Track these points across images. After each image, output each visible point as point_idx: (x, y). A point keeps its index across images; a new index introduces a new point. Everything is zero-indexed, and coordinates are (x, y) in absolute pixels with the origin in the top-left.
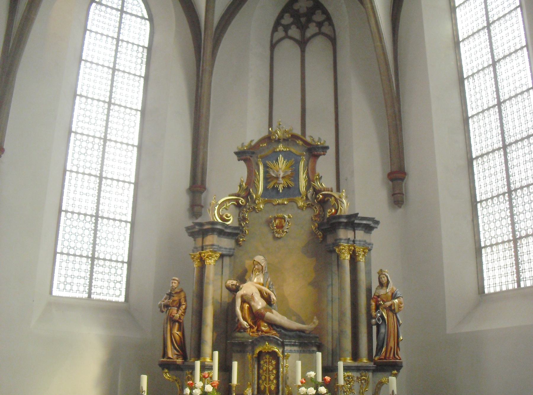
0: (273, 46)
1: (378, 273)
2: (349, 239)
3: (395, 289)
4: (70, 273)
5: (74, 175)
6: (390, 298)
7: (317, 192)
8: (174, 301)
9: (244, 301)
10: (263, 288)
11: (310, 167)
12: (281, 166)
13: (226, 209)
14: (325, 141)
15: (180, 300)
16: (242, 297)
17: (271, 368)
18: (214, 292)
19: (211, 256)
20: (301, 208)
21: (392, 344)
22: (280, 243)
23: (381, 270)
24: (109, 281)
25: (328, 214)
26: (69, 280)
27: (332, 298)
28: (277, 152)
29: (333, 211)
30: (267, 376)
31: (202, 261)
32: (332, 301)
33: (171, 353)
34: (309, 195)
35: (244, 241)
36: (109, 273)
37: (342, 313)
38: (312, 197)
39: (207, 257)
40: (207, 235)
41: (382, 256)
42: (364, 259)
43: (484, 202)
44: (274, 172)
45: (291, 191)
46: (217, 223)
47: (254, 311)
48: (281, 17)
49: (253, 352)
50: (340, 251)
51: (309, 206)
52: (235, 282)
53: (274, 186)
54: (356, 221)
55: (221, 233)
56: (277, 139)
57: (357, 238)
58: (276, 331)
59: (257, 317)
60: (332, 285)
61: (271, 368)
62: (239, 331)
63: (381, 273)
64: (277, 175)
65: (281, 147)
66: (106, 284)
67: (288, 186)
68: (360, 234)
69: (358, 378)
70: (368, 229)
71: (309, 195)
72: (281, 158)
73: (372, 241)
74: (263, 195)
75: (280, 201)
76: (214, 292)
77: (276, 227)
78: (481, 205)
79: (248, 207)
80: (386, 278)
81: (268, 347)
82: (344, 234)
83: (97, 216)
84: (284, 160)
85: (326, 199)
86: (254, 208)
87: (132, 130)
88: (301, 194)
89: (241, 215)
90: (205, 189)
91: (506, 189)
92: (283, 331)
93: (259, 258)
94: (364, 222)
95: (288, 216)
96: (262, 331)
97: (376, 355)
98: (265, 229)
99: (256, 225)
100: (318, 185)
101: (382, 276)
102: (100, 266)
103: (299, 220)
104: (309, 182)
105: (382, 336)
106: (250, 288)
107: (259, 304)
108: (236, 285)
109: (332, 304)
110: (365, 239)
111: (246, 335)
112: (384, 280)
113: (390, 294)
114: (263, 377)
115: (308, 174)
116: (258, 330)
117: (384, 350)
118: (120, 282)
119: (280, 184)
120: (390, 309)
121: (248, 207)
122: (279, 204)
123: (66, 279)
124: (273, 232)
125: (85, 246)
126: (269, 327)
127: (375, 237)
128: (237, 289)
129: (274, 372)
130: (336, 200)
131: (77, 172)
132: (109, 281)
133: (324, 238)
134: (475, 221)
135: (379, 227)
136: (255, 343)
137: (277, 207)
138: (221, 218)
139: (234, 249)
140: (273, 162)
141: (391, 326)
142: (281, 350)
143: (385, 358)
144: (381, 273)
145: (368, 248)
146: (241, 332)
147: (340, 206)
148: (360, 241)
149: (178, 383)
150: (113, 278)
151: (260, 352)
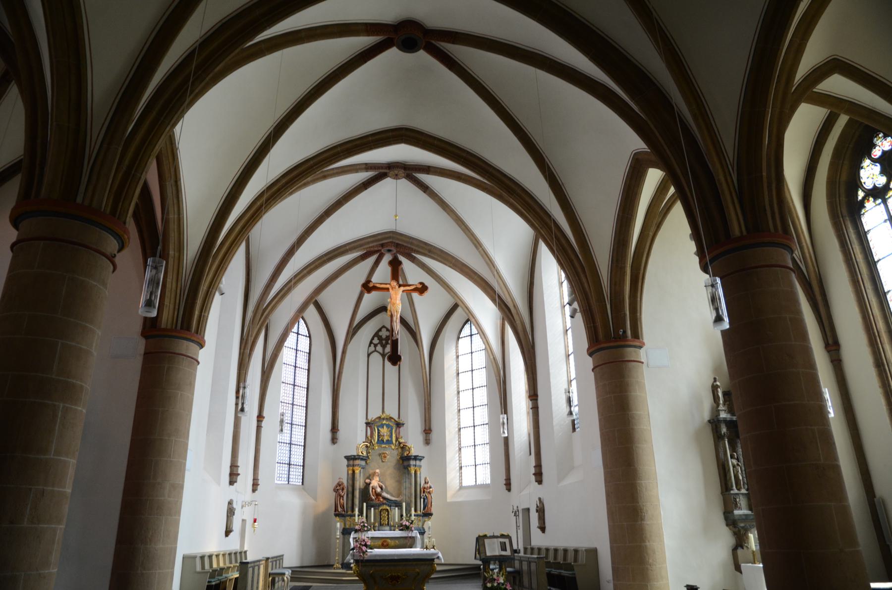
0: (369, 355)
7: (400, 443)
18: (360, 483)
31: (354, 471)
33: (340, 509)
37: (411, 494)
41: (424, 472)
48: (373, 339)
55: (362, 459)
59: (378, 495)
63: (425, 479)
65: (384, 422)
68: (418, 462)
76: (360, 483)
77: (382, 456)
81: (385, 507)
82: (412, 462)
83: (290, 444)
93: (378, 471)
100: (401, 441)
103: (392, 454)
104: (397, 439)
107: (379, 490)
120: (429, 493)
127: (423, 463)
134: (478, 279)
136: (379, 505)
144: (425, 479)
145: (420, 466)
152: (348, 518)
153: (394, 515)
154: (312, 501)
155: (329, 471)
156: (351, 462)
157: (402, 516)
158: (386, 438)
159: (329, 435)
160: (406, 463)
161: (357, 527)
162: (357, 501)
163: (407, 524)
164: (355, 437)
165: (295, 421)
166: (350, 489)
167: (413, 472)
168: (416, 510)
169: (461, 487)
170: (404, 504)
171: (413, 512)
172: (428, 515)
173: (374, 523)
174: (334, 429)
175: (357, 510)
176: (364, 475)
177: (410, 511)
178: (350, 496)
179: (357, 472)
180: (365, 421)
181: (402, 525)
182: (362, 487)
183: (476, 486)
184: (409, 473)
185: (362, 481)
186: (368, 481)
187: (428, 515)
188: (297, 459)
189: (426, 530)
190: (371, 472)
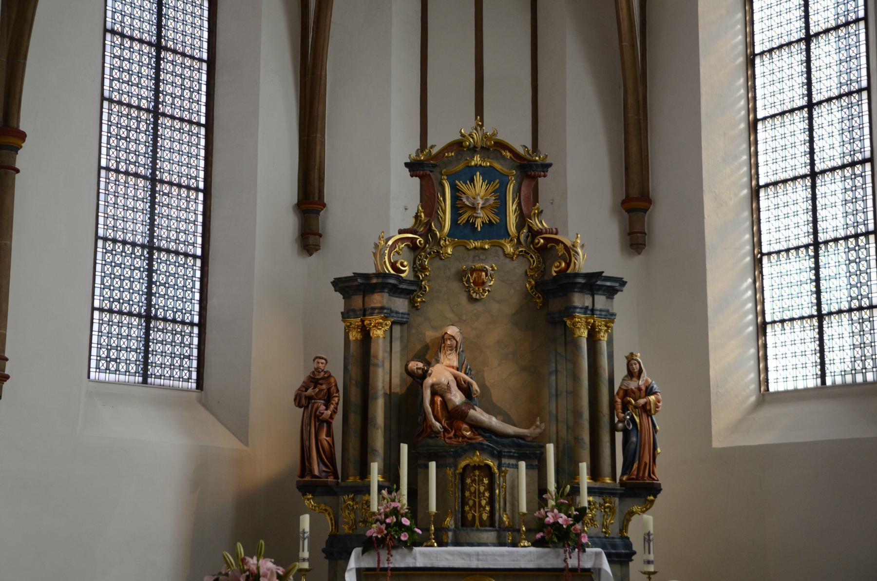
1: (627, 358)
2: (587, 307)
3: (650, 381)
4: (114, 342)
5: (113, 176)
6: (643, 394)
7: (534, 234)
8: (321, 390)
9: (434, 393)
10: (459, 373)
11: (522, 194)
12: (479, 191)
13: (398, 253)
14: (546, 156)
15: (329, 390)
16: (432, 386)
17: (482, 489)
18: (388, 374)
19: (381, 324)
20: (510, 257)
21: (647, 458)
22: (478, 307)
23: (632, 354)
24: (173, 356)
25: (554, 269)
26: (113, 354)
27: (557, 390)
28: (472, 166)
29: (563, 265)
30: (477, 500)
31: (366, 333)
32: (557, 396)
34: (522, 237)
35: (422, 302)
36: (173, 343)
37: (577, 414)
38: (526, 241)
39: (375, 326)
40: (373, 293)
41: (626, 335)
42: (606, 336)
43: (775, 256)
44: (468, 198)
45: (495, 230)
46: (390, 275)
47: (450, 407)
49: (456, 467)
50: (574, 324)
51: (524, 255)
52: (421, 365)
53: (468, 221)
54: (599, 283)
55: (395, 291)
56: (472, 146)
57: (598, 306)
58: (483, 436)
59: (455, 416)
60: (556, 371)
61: (482, 489)
62: (429, 437)
63: (630, 359)
64: (473, 204)
65: (477, 160)
66: (168, 361)
67: (490, 221)
68: (601, 301)
69: (601, 505)
70: (611, 292)
71: (522, 237)
72: (478, 178)
73: (615, 310)
74: (451, 234)
75: (478, 244)
76: (388, 374)
77: (470, 282)
78: (769, 259)
79: (428, 250)
80: (638, 365)
81: (477, 458)
82: (580, 300)
83: (151, 247)
84: (484, 181)
85: (549, 245)
86: (438, 252)
87: (195, 96)
88: (509, 235)
89: (418, 263)
90: (324, 205)
91: (810, 240)
92: (494, 437)
93: (452, 330)
94: (608, 284)
95: (492, 267)
96: (464, 437)
97: (623, 474)
98: (455, 286)
99: (441, 285)
100: (536, 224)
101: (633, 362)
102: (159, 330)
103: (505, 275)
104: (523, 220)
105: (633, 447)
106: (443, 372)
108: (423, 369)
109: (557, 400)
110: (606, 308)
111: (440, 441)
112: (636, 367)
113: (644, 388)
114: (471, 503)
115: (519, 204)
116: (455, 436)
117: (635, 466)
118: (188, 357)
119: (477, 217)
120: (646, 410)
121: (428, 250)
122: (475, 248)
123: (108, 353)
124: (469, 291)
125: (136, 298)
126: (472, 431)
127: (620, 303)
128: (425, 374)
129: (487, 494)
130: (566, 247)
131: (117, 171)
132: (173, 356)
133: (545, 303)
135: (625, 289)
136: (458, 454)
137: (472, 253)
138: (393, 266)
139: (408, 314)
140: (466, 183)
141: (645, 432)
142: (496, 463)
143: (637, 479)
144: (630, 359)
145: (610, 317)
146: (432, 438)
147: (573, 259)
148: (601, 310)
149: (329, 514)
150: (178, 350)
151: (465, 468)
152: (347, 499)
153: (515, 487)
154: (225, 441)
155: (282, 336)
156: (357, 302)
157: (543, 490)
158: (481, 217)
159: (288, 224)
160: (556, 305)
161: (373, 531)
162: (378, 440)
163: (562, 519)
164: (375, 209)
165: (168, 169)
166: (355, 395)
167: (584, 333)
168: (595, 473)
169: (766, 396)
170: (551, 448)
171: (585, 480)
172: (641, 489)
173: (439, 518)
174: (310, 200)
175: (375, 467)
176: (405, 348)
177: (576, 473)
178: (355, 419)
179: (378, 333)
180: (404, 147)
181: (541, 525)
182: (397, 388)
183: (823, 391)
184: (572, 343)
185: (397, 367)
186: (416, 365)
187: (641, 489)
188: (179, 294)
189: (637, 544)
190: (430, 335)
